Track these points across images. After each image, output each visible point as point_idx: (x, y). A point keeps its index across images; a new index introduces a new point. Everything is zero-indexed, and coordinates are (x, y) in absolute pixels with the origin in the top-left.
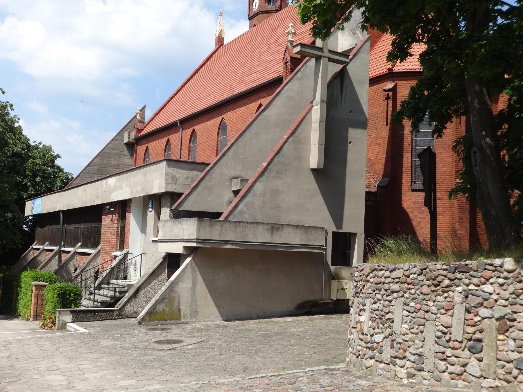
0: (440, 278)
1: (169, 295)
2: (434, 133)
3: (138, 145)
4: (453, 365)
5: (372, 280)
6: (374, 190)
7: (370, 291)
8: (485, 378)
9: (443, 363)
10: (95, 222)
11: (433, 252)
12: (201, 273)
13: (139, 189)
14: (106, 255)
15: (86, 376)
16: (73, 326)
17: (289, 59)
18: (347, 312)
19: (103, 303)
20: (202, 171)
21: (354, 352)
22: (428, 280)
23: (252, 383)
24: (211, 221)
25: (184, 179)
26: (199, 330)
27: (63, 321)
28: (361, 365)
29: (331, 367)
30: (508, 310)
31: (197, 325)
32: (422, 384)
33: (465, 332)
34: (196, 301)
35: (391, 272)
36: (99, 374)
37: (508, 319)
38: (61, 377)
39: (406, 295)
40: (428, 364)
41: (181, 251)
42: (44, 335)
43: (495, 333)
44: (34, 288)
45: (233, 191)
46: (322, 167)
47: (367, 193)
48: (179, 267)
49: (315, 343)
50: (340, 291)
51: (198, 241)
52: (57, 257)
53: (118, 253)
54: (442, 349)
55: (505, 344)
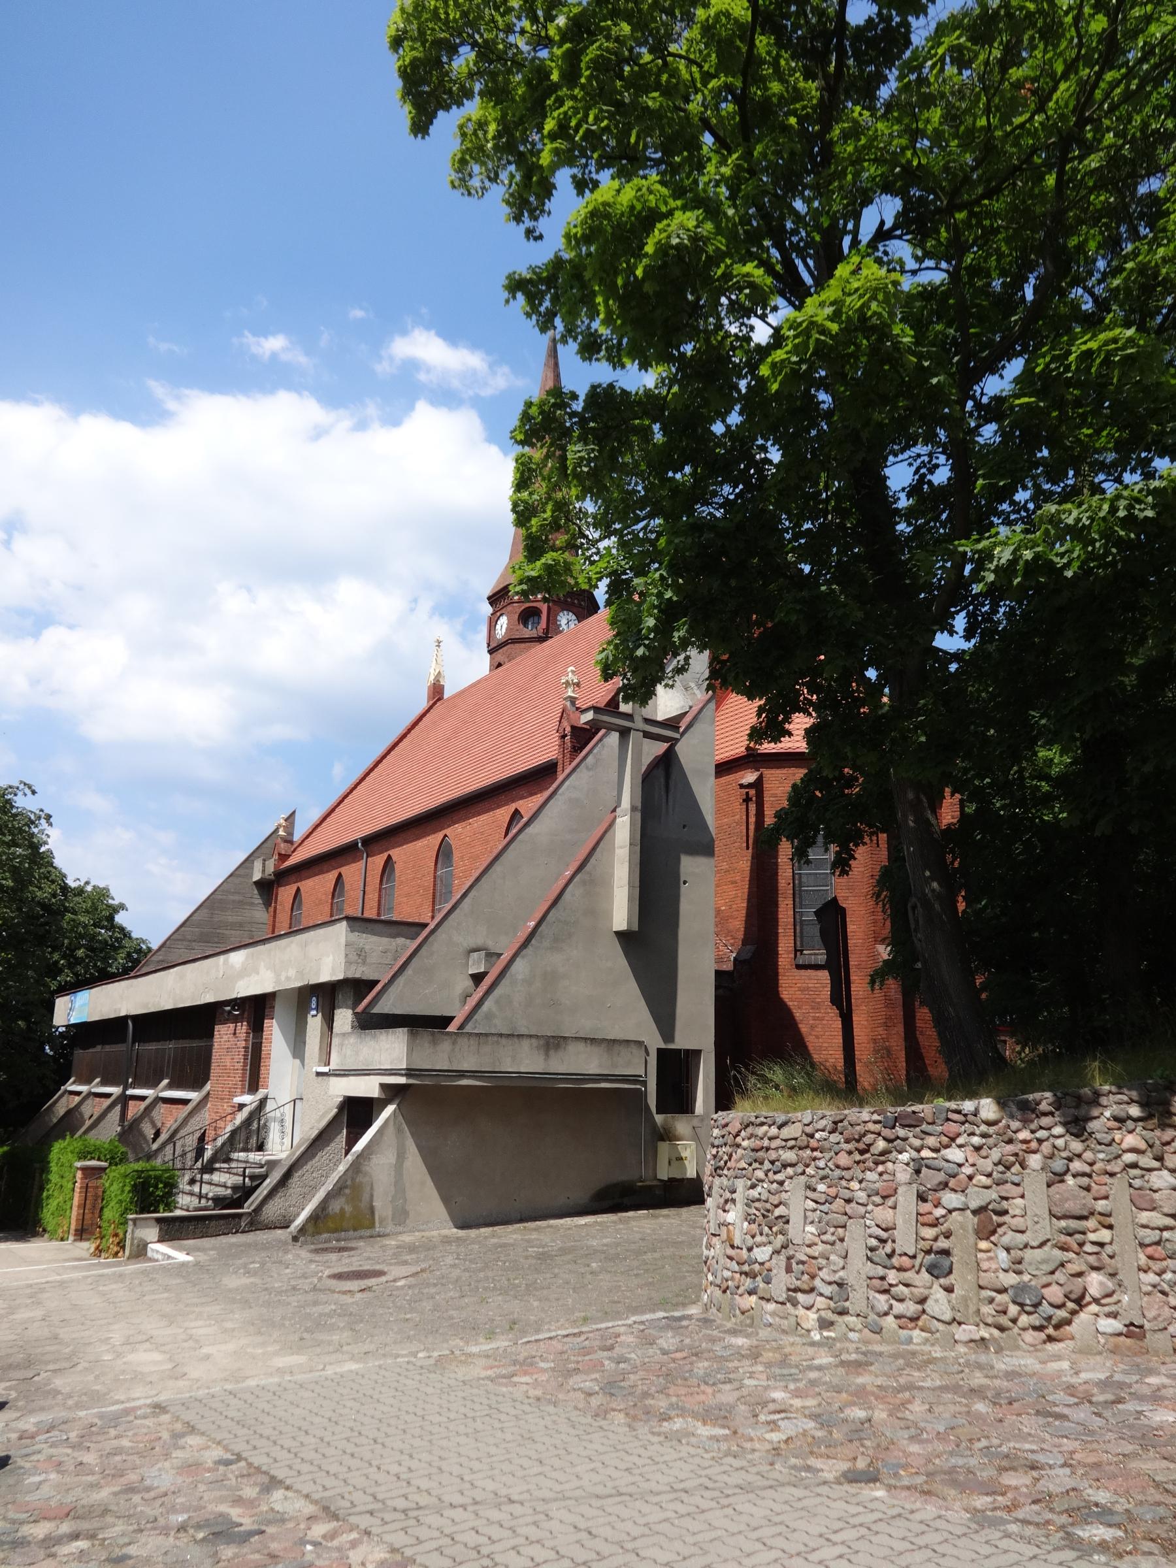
0: (869, 1138)
1: (353, 1179)
2: (834, 866)
3: (279, 885)
4: (901, 1300)
5: (745, 1144)
6: (728, 966)
7: (743, 1164)
8: (960, 1324)
9: (883, 1298)
10: (200, 1037)
11: (846, 1089)
12: (412, 1134)
13: (292, 973)
14: (221, 1104)
15: (205, 1350)
16: (160, 1250)
17: (568, 729)
18: (702, 1202)
19: (219, 1201)
20: (413, 938)
21: (718, 1281)
22: (847, 1141)
23: (532, 1350)
24: (433, 1034)
25: (379, 955)
26: (412, 1249)
27: (141, 1240)
28: (732, 1307)
29: (677, 1314)
30: (993, 1194)
31: (407, 1238)
32: (847, 1339)
33: (919, 1238)
34: (404, 1191)
35: (779, 1128)
36: (231, 1347)
37: (994, 1211)
38: (157, 1356)
39: (810, 1171)
40: (857, 1300)
41: (375, 1093)
42: (106, 1271)
43: (972, 1238)
44: (79, 1174)
45: (473, 976)
46: (635, 928)
47: (717, 973)
48: (370, 1125)
49: (638, 1268)
50: (674, 1163)
51: (409, 1072)
52: (118, 1108)
53: (246, 1099)
54: (880, 1271)
55: (990, 1259)
